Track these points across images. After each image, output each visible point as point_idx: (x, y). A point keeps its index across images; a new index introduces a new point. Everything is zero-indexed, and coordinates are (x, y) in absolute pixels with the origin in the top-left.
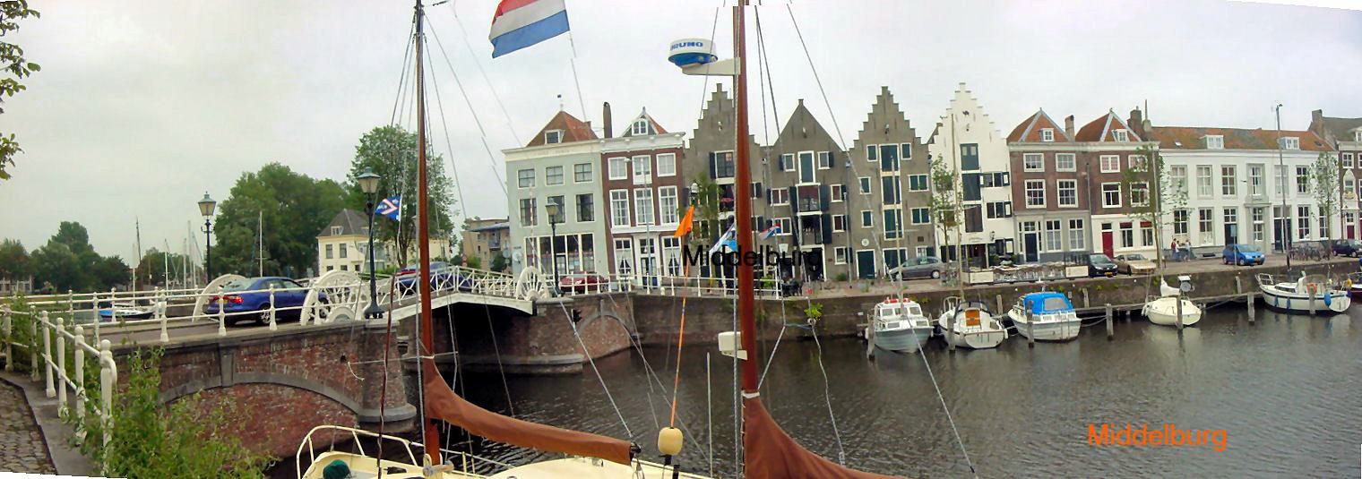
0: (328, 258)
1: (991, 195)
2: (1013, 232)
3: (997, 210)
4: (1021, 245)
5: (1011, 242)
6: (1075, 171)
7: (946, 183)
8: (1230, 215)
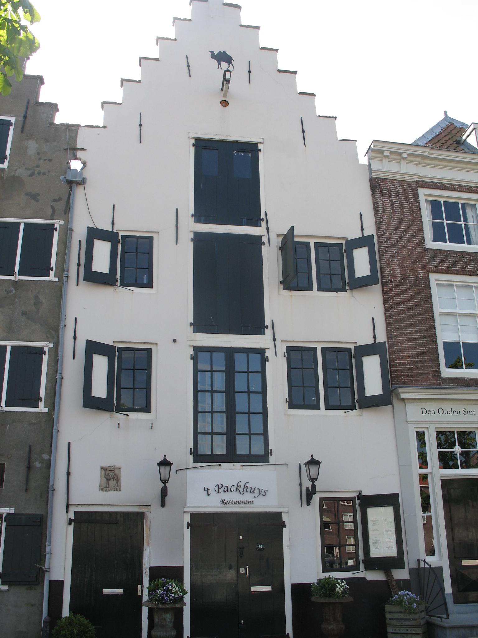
0: (243, 548)
1: (301, 318)
2: (402, 466)
3: (324, 377)
4: (428, 527)
5: (387, 512)
6: (427, 247)
7: (134, 262)
8: (457, 449)
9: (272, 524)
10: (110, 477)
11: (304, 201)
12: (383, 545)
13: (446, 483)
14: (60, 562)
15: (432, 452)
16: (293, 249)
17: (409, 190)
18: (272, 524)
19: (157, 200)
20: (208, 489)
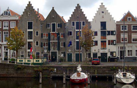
1: (110, 38)
3: (111, 42)
7: (96, 33)
9: (106, 54)
10: (95, 50)
11: (110, 27)
12: (114, 55)
13: (120, 51)
14: (92, 56)
15: (120, 48)
16: (109, 32)
17: (120, 25)
18: (106, 54)
19: (96, 28)
20: (102, 51)
